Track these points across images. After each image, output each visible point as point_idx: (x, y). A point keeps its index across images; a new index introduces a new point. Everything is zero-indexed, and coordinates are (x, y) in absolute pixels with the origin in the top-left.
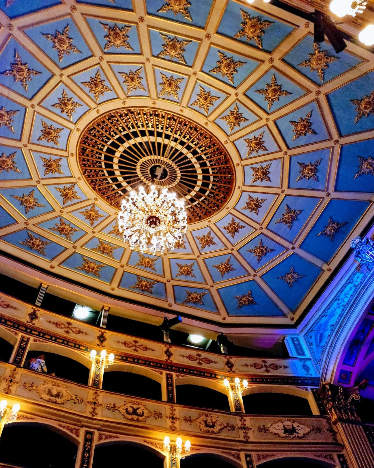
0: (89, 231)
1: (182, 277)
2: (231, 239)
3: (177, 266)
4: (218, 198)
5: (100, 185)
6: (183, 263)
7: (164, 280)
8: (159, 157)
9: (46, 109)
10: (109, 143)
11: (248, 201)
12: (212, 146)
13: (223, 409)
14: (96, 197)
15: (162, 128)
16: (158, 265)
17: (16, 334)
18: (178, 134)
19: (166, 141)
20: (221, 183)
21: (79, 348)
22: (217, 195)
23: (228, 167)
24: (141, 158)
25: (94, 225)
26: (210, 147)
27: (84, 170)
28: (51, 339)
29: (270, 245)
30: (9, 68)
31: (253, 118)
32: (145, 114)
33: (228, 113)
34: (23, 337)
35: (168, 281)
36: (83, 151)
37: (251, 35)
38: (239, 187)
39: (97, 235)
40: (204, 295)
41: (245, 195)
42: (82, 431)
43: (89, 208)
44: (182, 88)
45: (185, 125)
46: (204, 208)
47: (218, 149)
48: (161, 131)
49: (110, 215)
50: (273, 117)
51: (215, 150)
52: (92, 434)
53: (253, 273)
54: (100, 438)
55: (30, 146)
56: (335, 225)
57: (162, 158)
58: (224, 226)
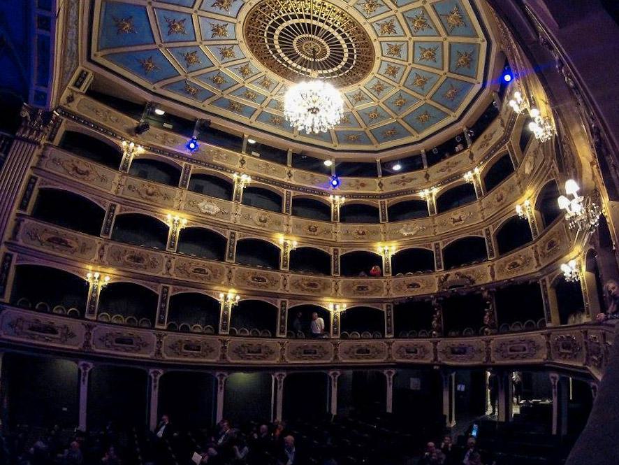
8: (307, 36)
10: (270, 23)
21: (226, 171)
48: (317, 16)
54: (121, 210)
56: (454, 91)
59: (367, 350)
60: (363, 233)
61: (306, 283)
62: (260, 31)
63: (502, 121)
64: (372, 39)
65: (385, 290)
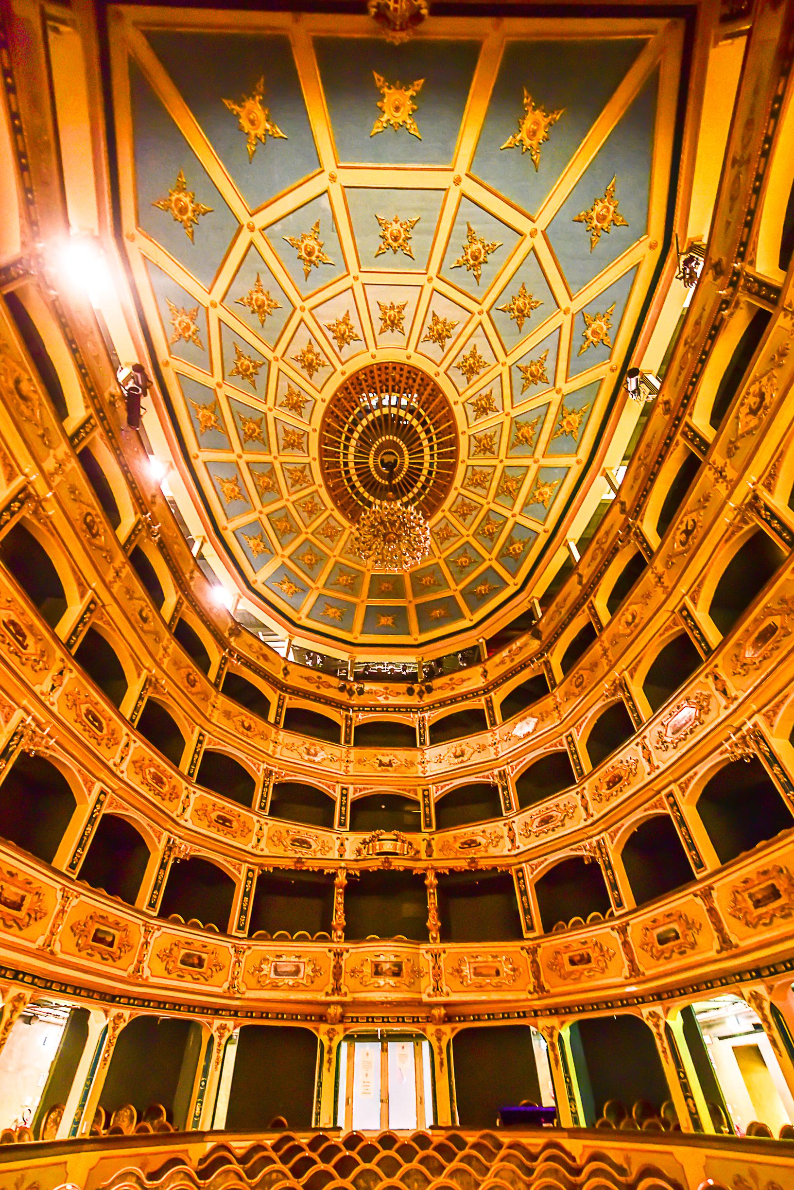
4: (398, 377)
13: (533, 614)
17: (480, 700)
19: (351, 465)
22: (394, 380)
28: (371, 710)
34: (486, 699)
42: (338, 788)
52: (347, 789)
59: (200, 958)
60: (249, 728)
61: (153, 770)
62: (387, 386)
63: (485, 671)
64: (443, 508)
65: (255, 839)
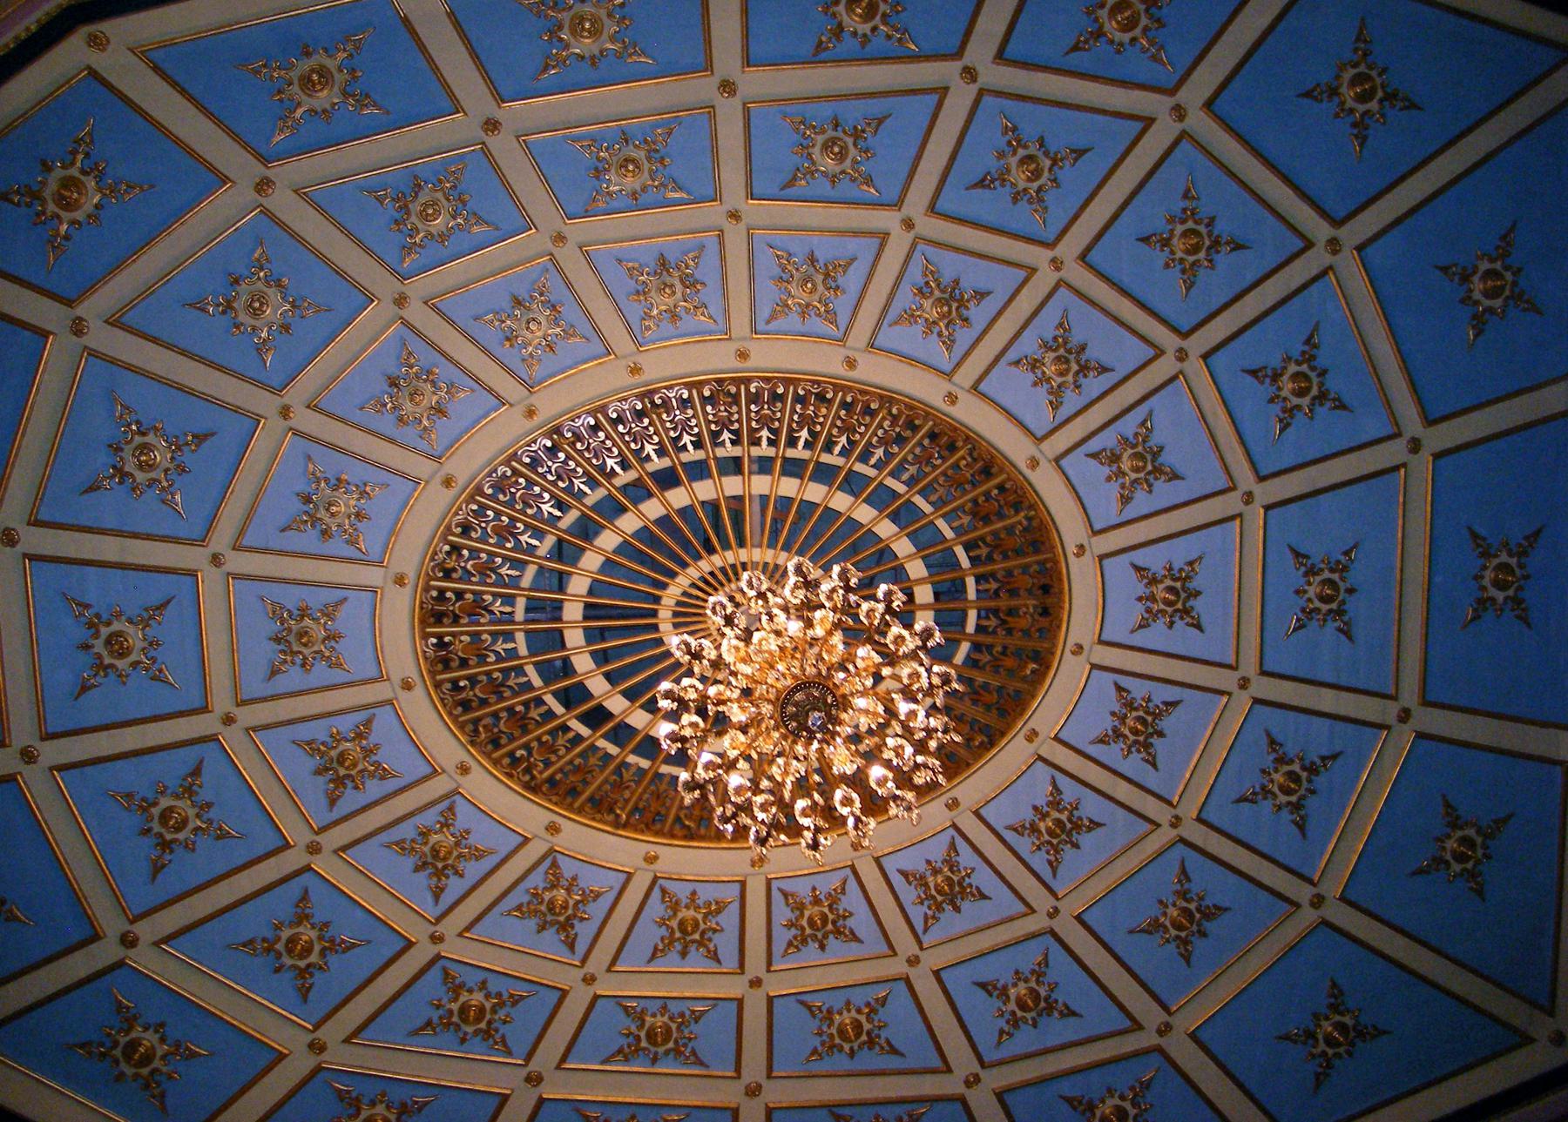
0: (567, 978)
1: (1025, 1039)
2: (1151, 779)
3: (981, 993)
5: (548, 764)
6: (998, 970)
7: (950, 1085)
9: (265, 551)
11: (1141, 589)
12: (908, 433)
14: (548, 817)
15: (698, 445)
16: (899, 1023)
18: (764, 443)
20: (1006, 557)
23: (1001, 487)
24: (664, 586)
25: (581, 947)
26: (900, 440)
27: (470, 727)
29: (1314, 739)
30: (103, 458)
31: (1000, 281)
32: (620, 420)
33: (906, 297)
35: (968, 1084)
36: (441, 659)
37: (865, 28)
38: (1081, 547)
39: (607, 987)
40: (1147, 1086)
41: (1119, 569)
43: (537, 880)
44: (712, 280)
45: (775, 397)
46: (986, 686)
47: (933, 436)
49: (629, 876)
50: (1070, 247)
51: (926, 442)
53: (1304, 893)
55: (247, 716)
57: (743, 555)
58: (1096, 733)
